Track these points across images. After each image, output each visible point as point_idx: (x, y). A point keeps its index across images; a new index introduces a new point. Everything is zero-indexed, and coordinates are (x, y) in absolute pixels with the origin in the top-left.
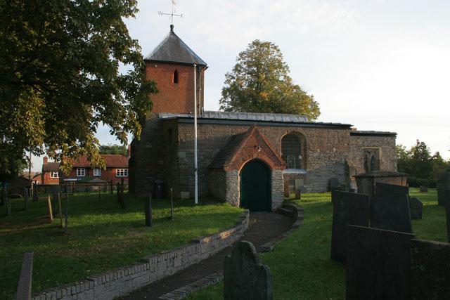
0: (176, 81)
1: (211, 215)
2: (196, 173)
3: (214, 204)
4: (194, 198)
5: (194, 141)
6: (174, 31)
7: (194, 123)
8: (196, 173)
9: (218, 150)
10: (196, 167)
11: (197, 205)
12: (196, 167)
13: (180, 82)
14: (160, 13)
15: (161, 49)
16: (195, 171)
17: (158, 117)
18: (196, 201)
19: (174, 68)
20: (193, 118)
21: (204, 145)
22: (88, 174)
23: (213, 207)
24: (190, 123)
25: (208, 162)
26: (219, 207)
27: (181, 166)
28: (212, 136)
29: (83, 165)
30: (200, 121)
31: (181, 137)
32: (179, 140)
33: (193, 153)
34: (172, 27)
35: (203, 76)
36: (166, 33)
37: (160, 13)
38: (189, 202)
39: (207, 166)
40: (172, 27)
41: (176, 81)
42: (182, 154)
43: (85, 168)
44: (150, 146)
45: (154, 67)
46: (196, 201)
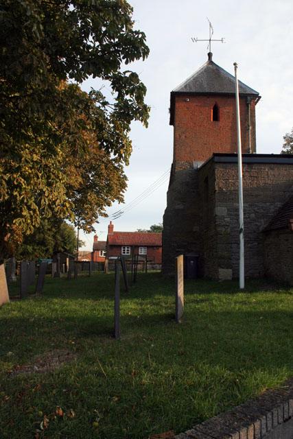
0: (216, 118)
1: (266, 315)
2: (242, 236)
3: (273, 291)
4: (238, 279)
5: (237, 191)
6: (214, 60)
7: (237, 163)
8: (242, 236)
9: (279, 205)
10: (242, 226)
11: (242, 291)
12: (242, 226)
13: (221, 120)
14: (195, 40)
15: (196, 80)
16: (240, 232)
17: (192, 166)
18: (242, 285)
19: (212, 101)
20: (237, 155)
21: (257, 196)
22: (132, 252)
23: (270, 295)
24: (230, 163)
25: (263, 224)
26: (283, 296)
27: (219, 229)
28: (269, 182)
29: (129, 243)
30: (248, 160)
31: (219, 184)
32: (217, 189)
33: (237, 210)
34: (210, 55)
35: (253, 116)
36: (202, 62)
37: (195, 40)
38: (231, 286)
39: (261, 229)
40: (210, 55)
41: (216, 118)
42: (221, 210)
43: (131, 246)
44: (181, 207)
45: (186, 101)
46: (242, 285)
